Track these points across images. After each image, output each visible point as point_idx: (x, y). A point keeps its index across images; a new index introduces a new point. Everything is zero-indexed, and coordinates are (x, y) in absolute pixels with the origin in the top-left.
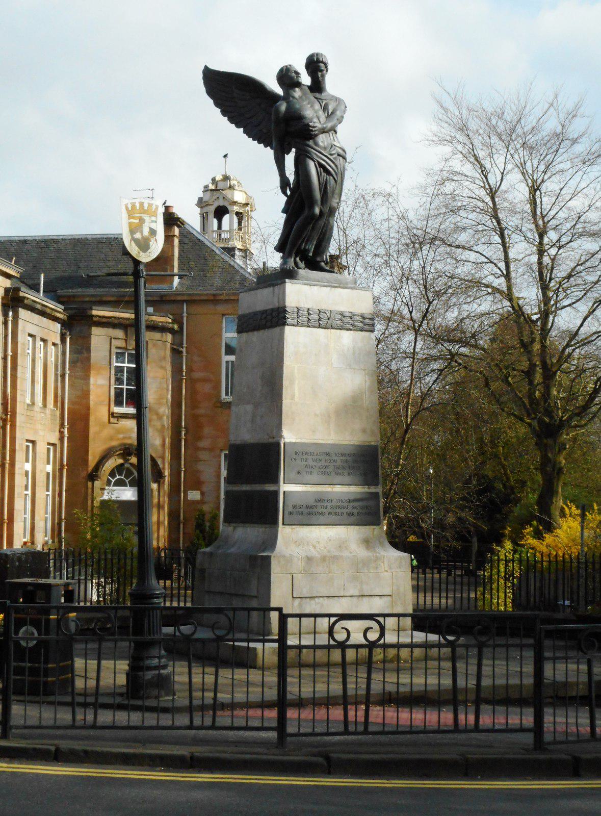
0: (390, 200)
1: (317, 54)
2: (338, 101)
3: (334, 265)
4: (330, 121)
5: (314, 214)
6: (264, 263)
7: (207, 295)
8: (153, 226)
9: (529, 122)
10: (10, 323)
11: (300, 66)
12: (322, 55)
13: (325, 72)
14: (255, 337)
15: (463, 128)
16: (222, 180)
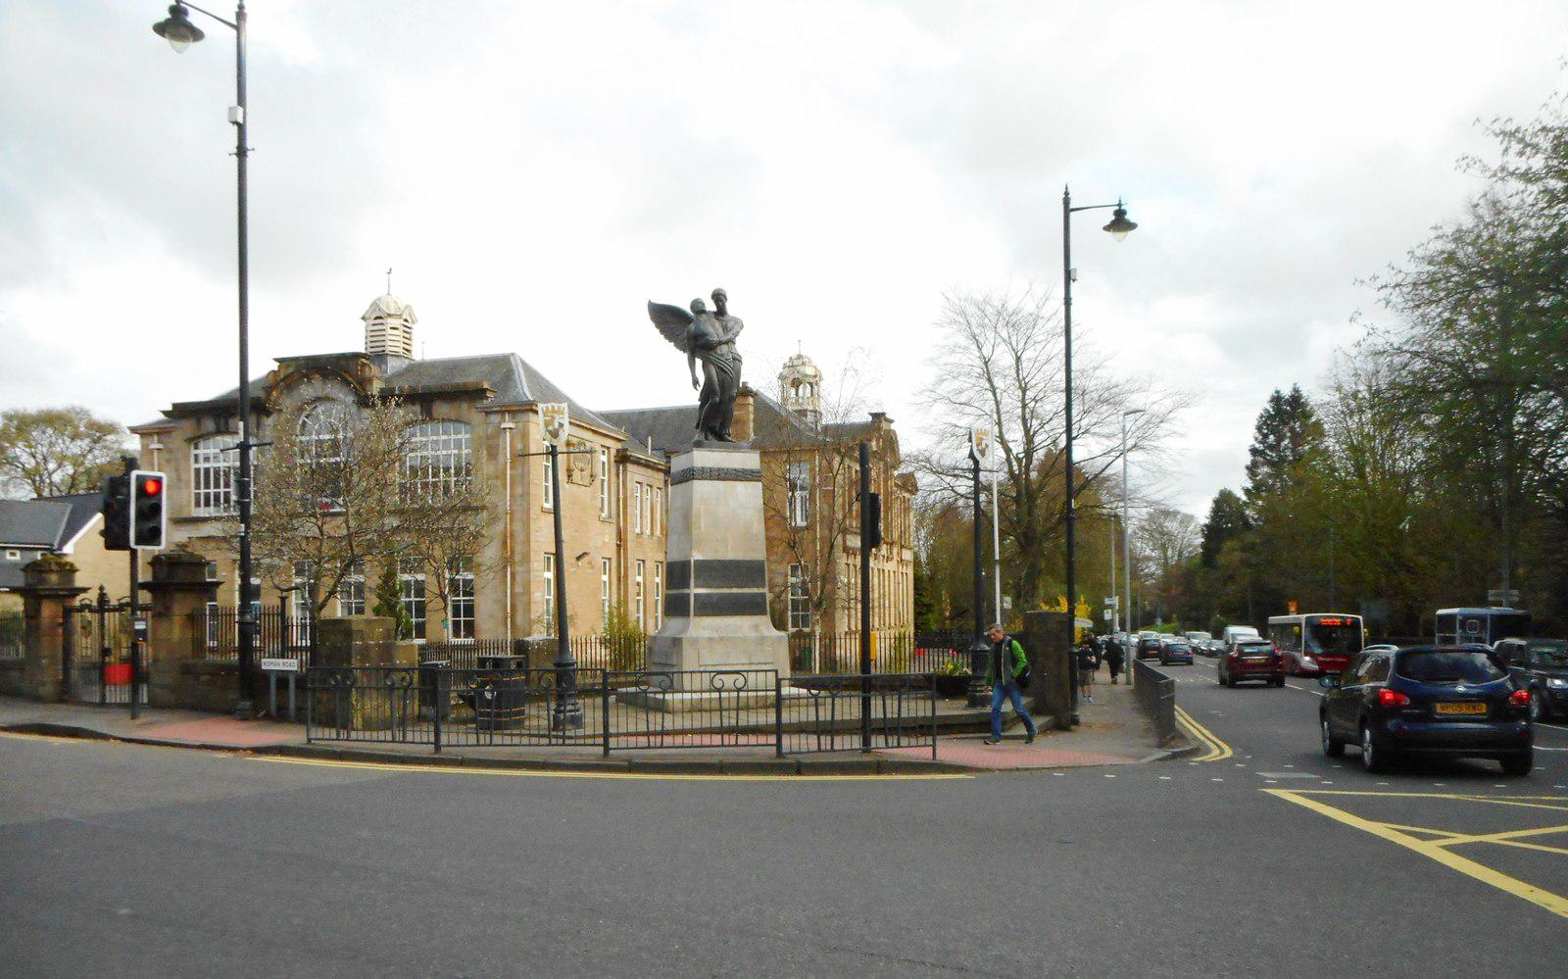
8: (562, 421)
9: (1011, 307)
10: (621, 475)
15: (963, 313)
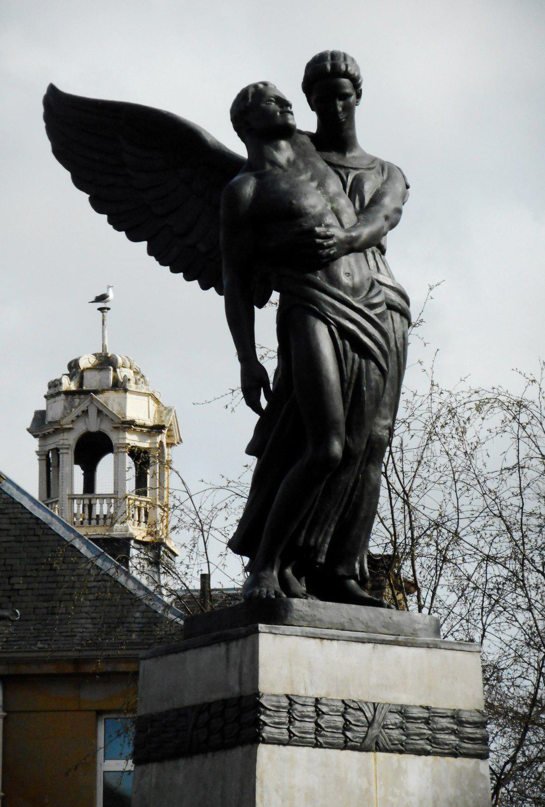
0: (524, 418)
1: (334, 56)
2: (387, 170)
3: (383, 583)
4: (367, 222)
5: (329, 458)
6: (205, 579)
7: (55, 661)
11: (290, 87)
12: (345, 57)
13: (353, 98)
14: (181, 773)
16: (93, 368)
